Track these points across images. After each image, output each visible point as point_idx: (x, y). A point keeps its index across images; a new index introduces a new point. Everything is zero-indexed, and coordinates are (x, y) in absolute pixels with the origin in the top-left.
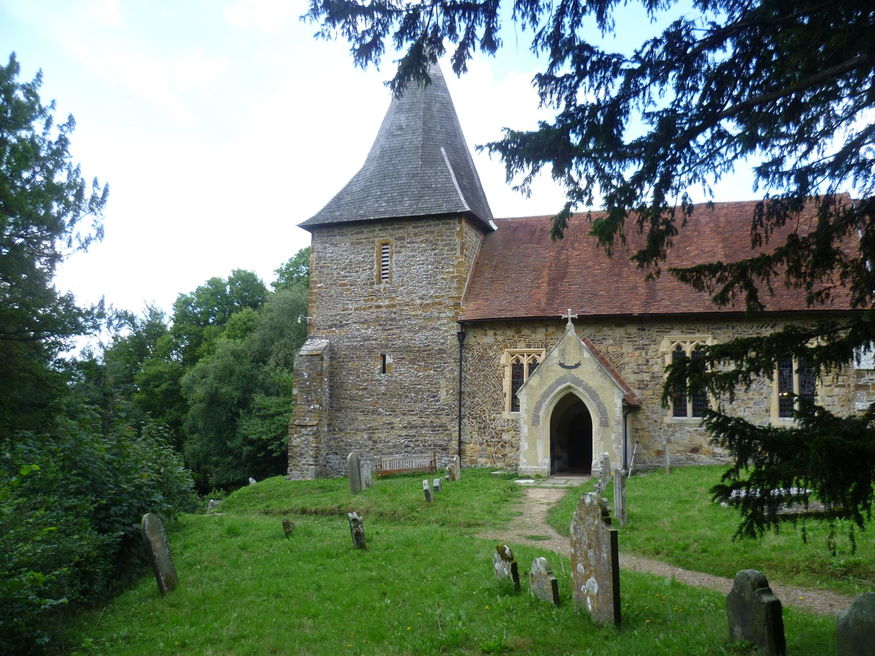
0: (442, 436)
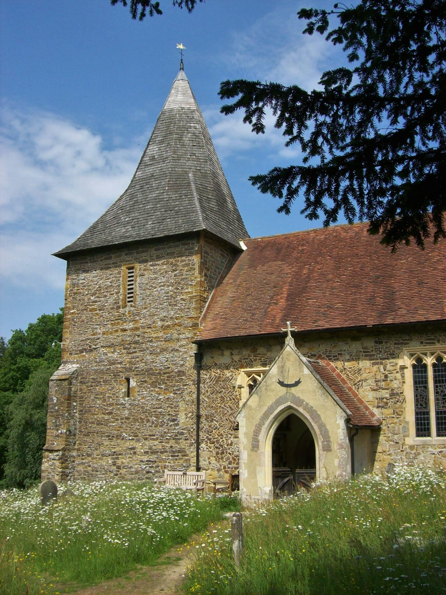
0: (181, 461)
